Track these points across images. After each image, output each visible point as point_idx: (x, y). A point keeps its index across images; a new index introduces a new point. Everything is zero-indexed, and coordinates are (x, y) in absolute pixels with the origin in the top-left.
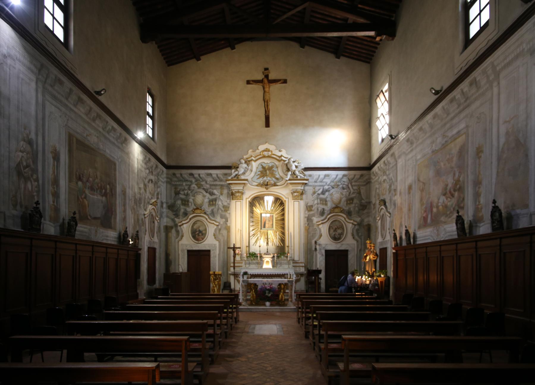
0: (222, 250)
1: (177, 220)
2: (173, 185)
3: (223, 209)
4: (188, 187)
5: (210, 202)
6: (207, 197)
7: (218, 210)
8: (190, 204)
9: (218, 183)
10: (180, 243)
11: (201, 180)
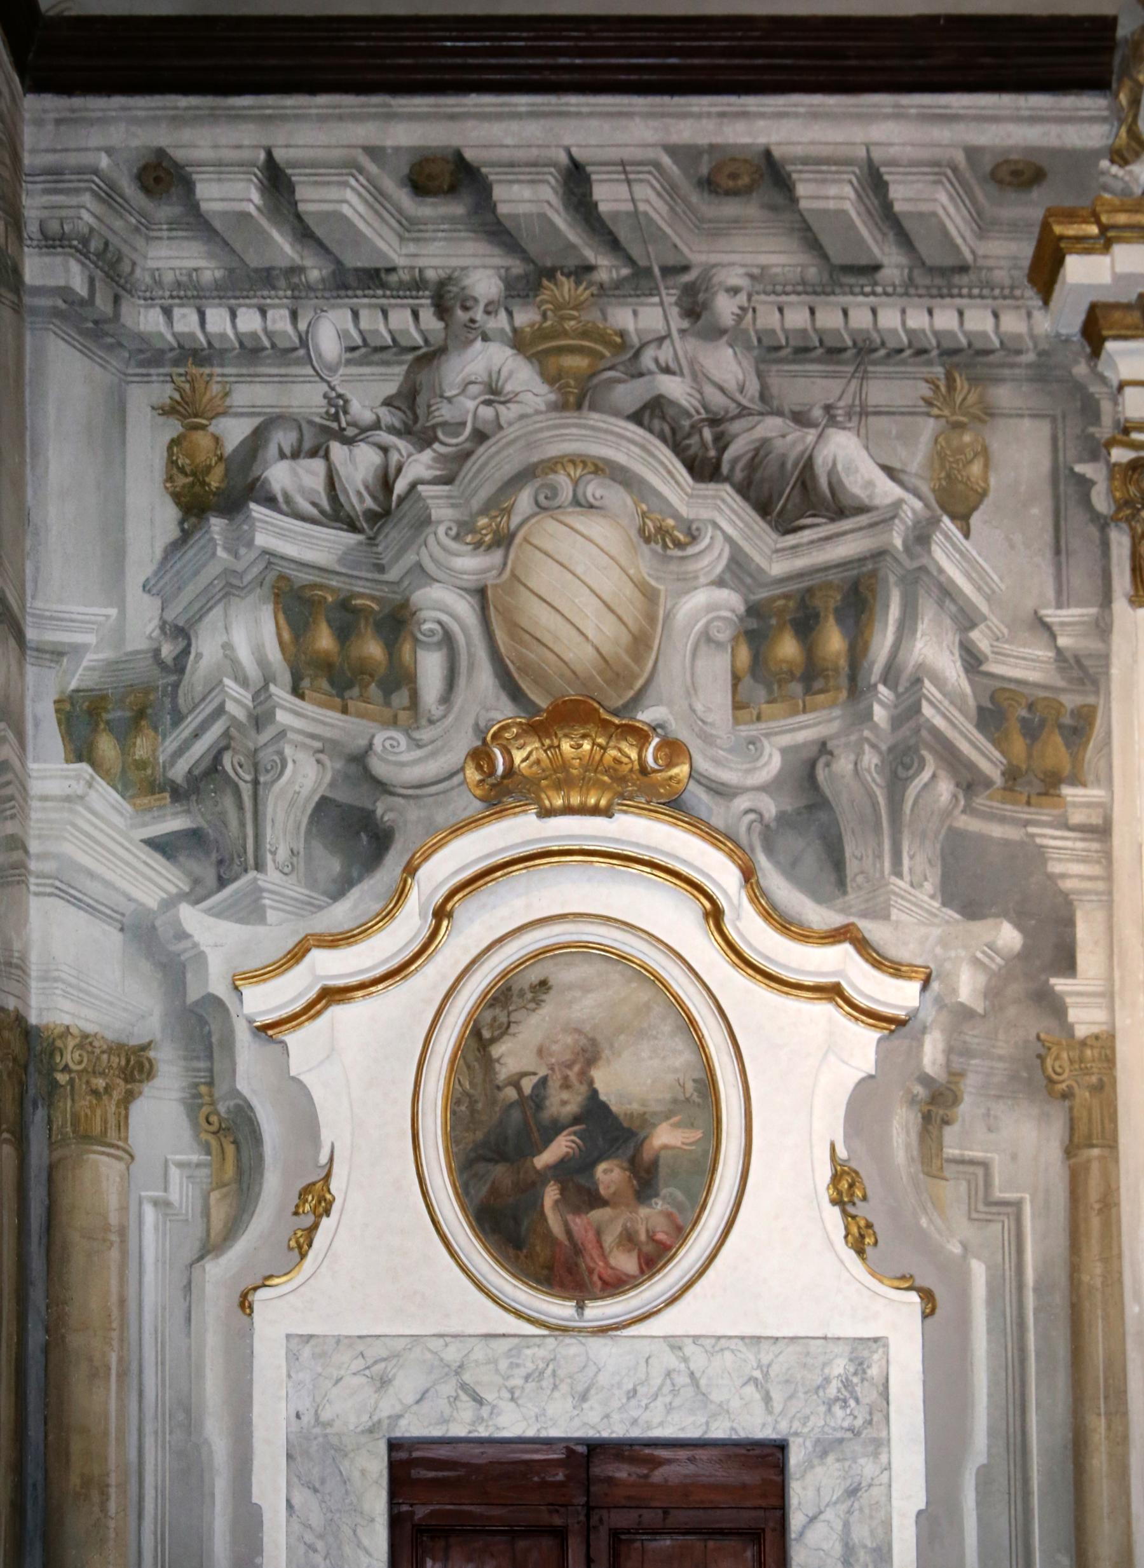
0: (979, 1445)
1: (216, 938)
2: (150, 356)
3: (987, 760)
4: (389, 380)
5: (756, 628)
6: (711, 558)
7: (901, 763)
8: (430, 668)
9: (897, 319)
10: (278, 1315)
11: (607, 269)
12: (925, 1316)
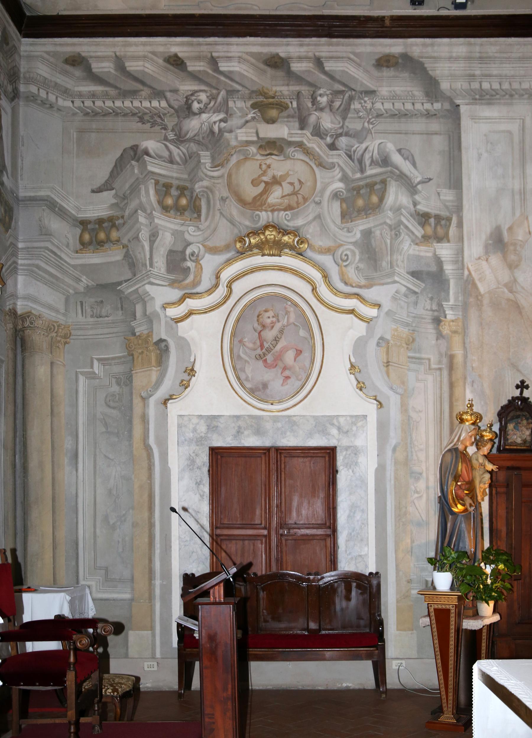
12: (378, 409)
